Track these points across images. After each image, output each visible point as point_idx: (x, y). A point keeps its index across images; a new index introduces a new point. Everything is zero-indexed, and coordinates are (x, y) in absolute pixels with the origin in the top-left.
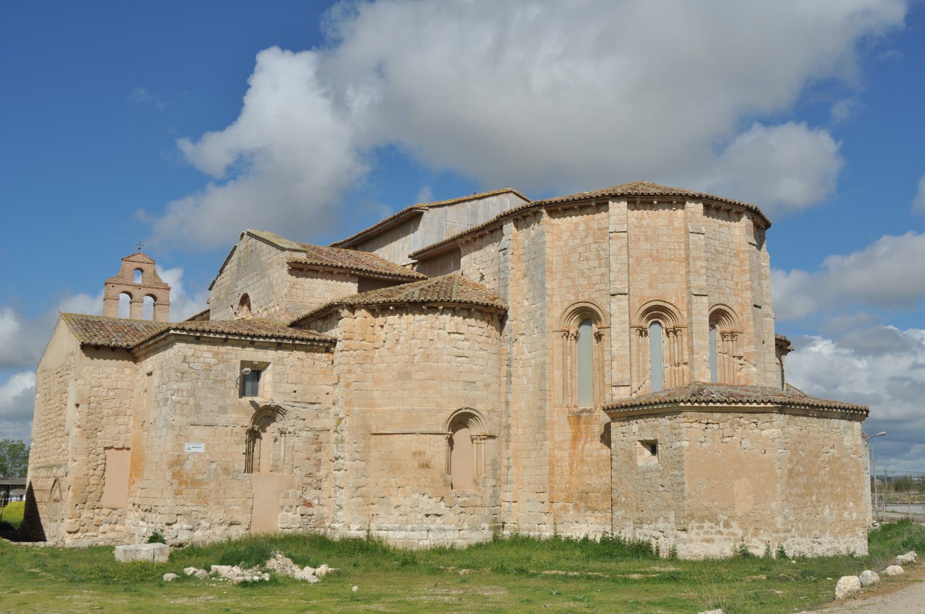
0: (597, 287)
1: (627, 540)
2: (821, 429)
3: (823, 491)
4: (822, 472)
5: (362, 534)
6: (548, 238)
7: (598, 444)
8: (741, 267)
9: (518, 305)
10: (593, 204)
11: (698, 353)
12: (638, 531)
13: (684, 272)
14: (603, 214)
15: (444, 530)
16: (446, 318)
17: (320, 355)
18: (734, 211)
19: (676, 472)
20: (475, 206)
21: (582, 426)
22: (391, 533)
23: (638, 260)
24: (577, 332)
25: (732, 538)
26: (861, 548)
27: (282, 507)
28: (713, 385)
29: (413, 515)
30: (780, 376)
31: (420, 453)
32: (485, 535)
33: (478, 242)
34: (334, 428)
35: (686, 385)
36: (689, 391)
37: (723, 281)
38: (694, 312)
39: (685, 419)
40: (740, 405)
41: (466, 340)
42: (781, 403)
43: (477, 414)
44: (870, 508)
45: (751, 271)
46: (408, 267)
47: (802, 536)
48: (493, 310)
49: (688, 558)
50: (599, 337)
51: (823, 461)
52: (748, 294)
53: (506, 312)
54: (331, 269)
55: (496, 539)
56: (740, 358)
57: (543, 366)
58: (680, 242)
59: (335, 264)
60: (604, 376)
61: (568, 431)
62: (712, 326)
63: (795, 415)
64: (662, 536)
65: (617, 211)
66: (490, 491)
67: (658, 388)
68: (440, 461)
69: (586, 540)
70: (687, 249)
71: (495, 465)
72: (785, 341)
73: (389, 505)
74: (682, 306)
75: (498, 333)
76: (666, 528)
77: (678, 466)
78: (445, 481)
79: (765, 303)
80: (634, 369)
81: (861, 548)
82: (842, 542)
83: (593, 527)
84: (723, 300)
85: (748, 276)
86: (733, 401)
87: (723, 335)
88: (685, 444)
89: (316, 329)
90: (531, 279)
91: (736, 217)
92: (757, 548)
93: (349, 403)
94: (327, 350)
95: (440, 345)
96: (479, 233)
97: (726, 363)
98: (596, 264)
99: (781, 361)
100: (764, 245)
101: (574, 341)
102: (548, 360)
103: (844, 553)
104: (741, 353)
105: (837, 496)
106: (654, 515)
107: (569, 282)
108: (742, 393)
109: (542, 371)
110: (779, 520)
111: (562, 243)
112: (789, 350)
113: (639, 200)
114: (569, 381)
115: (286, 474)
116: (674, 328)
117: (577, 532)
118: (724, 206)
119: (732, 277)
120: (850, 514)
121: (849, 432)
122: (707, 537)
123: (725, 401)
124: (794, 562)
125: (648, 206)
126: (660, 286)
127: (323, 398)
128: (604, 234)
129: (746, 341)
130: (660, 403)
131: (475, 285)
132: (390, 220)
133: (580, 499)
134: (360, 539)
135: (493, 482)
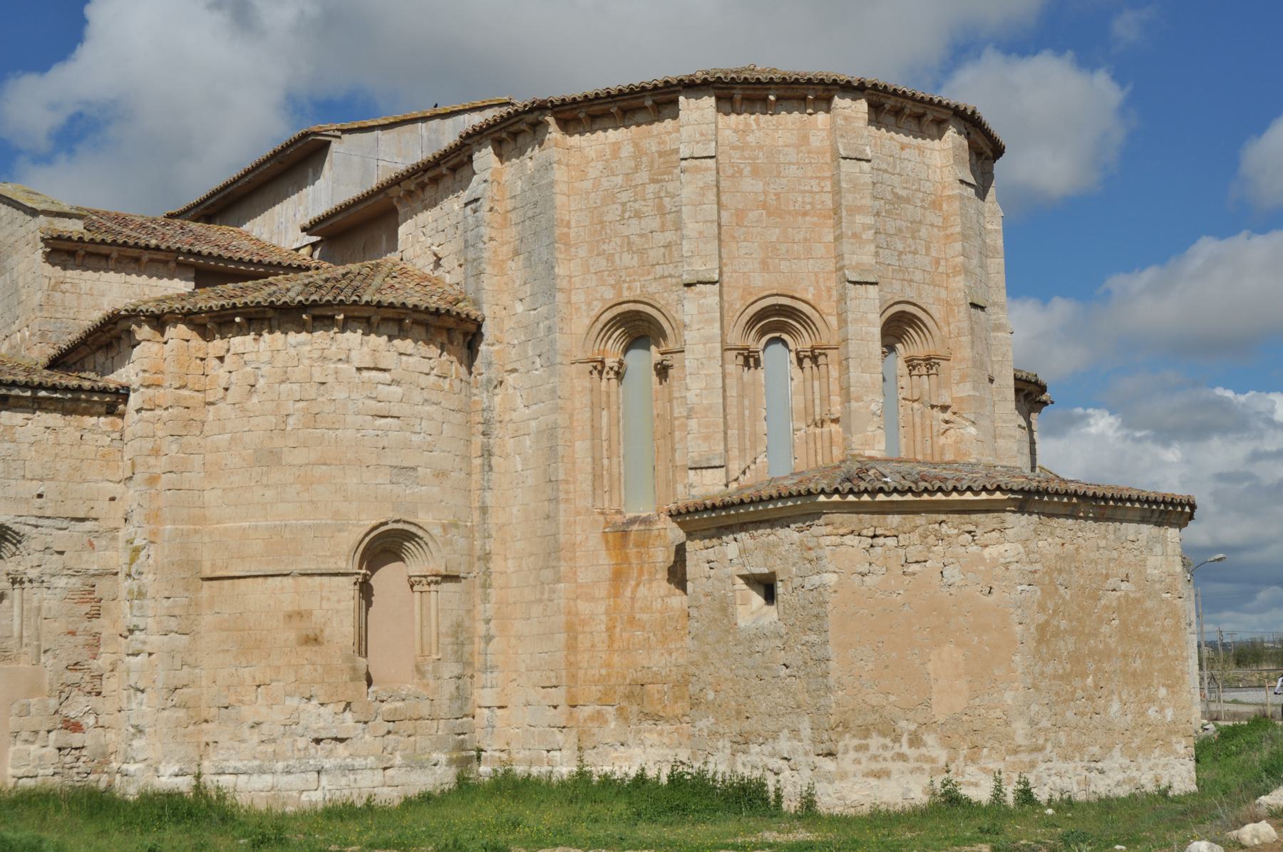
0: (659, 270)
1: (719, 777)
2: (1103, 543)
3: (1106, 666)
4: (1105, 629)
5: (184, 785)
6: (559, 174)
7: (662, 585)
8: (945, 228)
9: (503, 312)
10: (649, 103)
11: (859, 399)
12: (741, 758)
13: (831, 238)
14: (669, 123)
15: (353, 770)
16: (353, 338)
17: (94, 420)
18: (930, 117)
19: (813, 638)
20: (436, 131)
21: (632, 551)
22: (243, 778)
23: (740, 215)
24: (621, 363)
25: (927, 766)
26: (1181, 775)
27: (16, 734)
28: (887, 461)
29: (287, 740)
30: (1027, 451)
31: (300, 614)
32: (441, 776)
33: (430, 192)
34: (125, 569)
35: (836, 463)
36: (840, 474)
37: (910, 256)
38: (850, 316)
39: (829, 529)
40: (939, 496)
41: (394, 382)
42: (1022, 491)
43: (420, 533)
44: (1198, 697)
45: (965, 237)
46: (304, 252)
47: (1066, 758)
48: (450, 323)
49: (837, 811)
50: (662, 371)
51: (1106, 607)
52: (959, 282)
53: (480, 326)
54: (136, 253)
55: (463, 785)
56: (945, 408)
57: (551, 432)
58: (823, 178)
59: (142, 243)
60: (673, 450)
61: (605, 560)
62: (889, 348)
63: (1050, 516)
64: (787, 768)
65: (696, 115)
66: (449, 688)
67: (782, 470)
68: (342, 629)
69: (641, 780)
70: (837, 191)
71: (460, 635)
72: (1036, 383)
73: (239, 722)
74: (828, 306)
75: (463, 370)
76: (794, 751)
77: (815, 624)
78: (354, 669)
79: (994, 304)
80: (733, 433)
81: (1181, 775)
82: (1145, 767)
83: (655, 753)
84: (910, 294)
85: (958, 246)
86: (926, 490)
87: (911, 363)
88: (830, 579)
89: (94, 370)
90: (529, 259)
91: (934, 130)
92: (976, 785)
93: (154, 516)
94: (111, 410)
95: (340, 394)
96: (431, 174)
97: (917, 420)
98: (655, 223)
99: (1029, 424)
100: (992, 191)
101: (614, 382)
102: (562, 419)
103: (1150, 788)
104: (946, 400)
105: (1134, 674)
106: (771, 725)
107: (602, 263)
108: (945, 473)
109: (551, 444)
110: (1020, 729)
111: (587, 185)
112: (1045, 403)
113: (740, 93)
114: (606, 462)
115: (24, 665)
116: (813, 349)
117: (622, 762)
118: (909, 107)
119: (928, 249)
120: (1161, 710)
121: (1158, 549)
122: (875, 766)
123: (910, 490)
124: (1050, 811)
125: (758, 106)
126: (784, 265)
127: (102, 507)
128: (670, 163)
129: (956, 375)
130: (780, 497)
131: (426, 278)
132: (268, 159)
133: (629, 696)
134: (181, 794)
135: (456, 669)
